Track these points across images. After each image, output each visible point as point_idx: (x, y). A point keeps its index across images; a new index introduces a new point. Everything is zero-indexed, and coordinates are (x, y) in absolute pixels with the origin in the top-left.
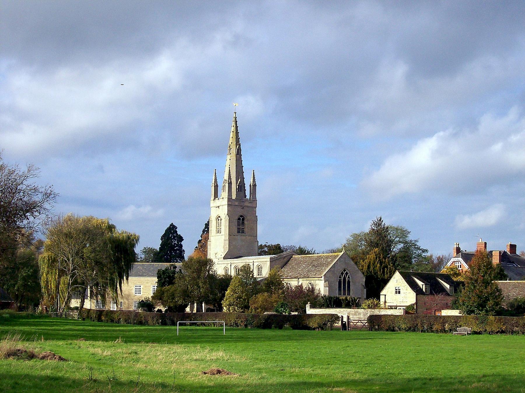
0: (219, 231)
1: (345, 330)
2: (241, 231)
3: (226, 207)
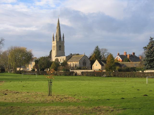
0: (54, 50)
1: (76, 76)
2: (60, 50)
3: (56, 43)
